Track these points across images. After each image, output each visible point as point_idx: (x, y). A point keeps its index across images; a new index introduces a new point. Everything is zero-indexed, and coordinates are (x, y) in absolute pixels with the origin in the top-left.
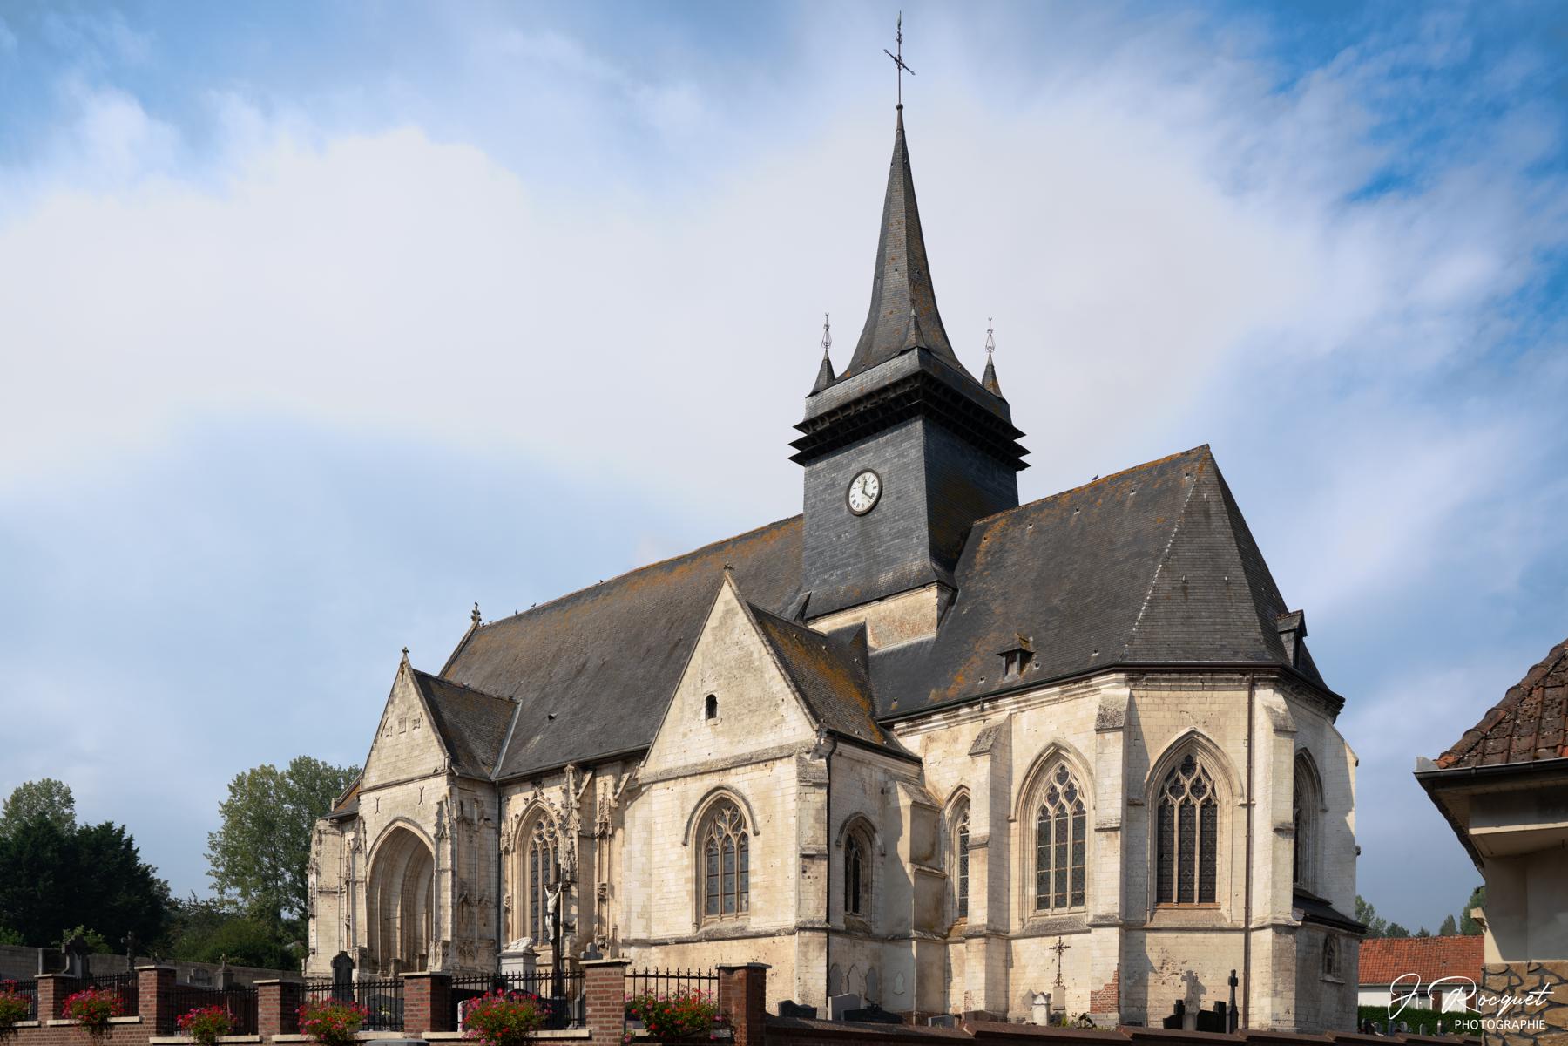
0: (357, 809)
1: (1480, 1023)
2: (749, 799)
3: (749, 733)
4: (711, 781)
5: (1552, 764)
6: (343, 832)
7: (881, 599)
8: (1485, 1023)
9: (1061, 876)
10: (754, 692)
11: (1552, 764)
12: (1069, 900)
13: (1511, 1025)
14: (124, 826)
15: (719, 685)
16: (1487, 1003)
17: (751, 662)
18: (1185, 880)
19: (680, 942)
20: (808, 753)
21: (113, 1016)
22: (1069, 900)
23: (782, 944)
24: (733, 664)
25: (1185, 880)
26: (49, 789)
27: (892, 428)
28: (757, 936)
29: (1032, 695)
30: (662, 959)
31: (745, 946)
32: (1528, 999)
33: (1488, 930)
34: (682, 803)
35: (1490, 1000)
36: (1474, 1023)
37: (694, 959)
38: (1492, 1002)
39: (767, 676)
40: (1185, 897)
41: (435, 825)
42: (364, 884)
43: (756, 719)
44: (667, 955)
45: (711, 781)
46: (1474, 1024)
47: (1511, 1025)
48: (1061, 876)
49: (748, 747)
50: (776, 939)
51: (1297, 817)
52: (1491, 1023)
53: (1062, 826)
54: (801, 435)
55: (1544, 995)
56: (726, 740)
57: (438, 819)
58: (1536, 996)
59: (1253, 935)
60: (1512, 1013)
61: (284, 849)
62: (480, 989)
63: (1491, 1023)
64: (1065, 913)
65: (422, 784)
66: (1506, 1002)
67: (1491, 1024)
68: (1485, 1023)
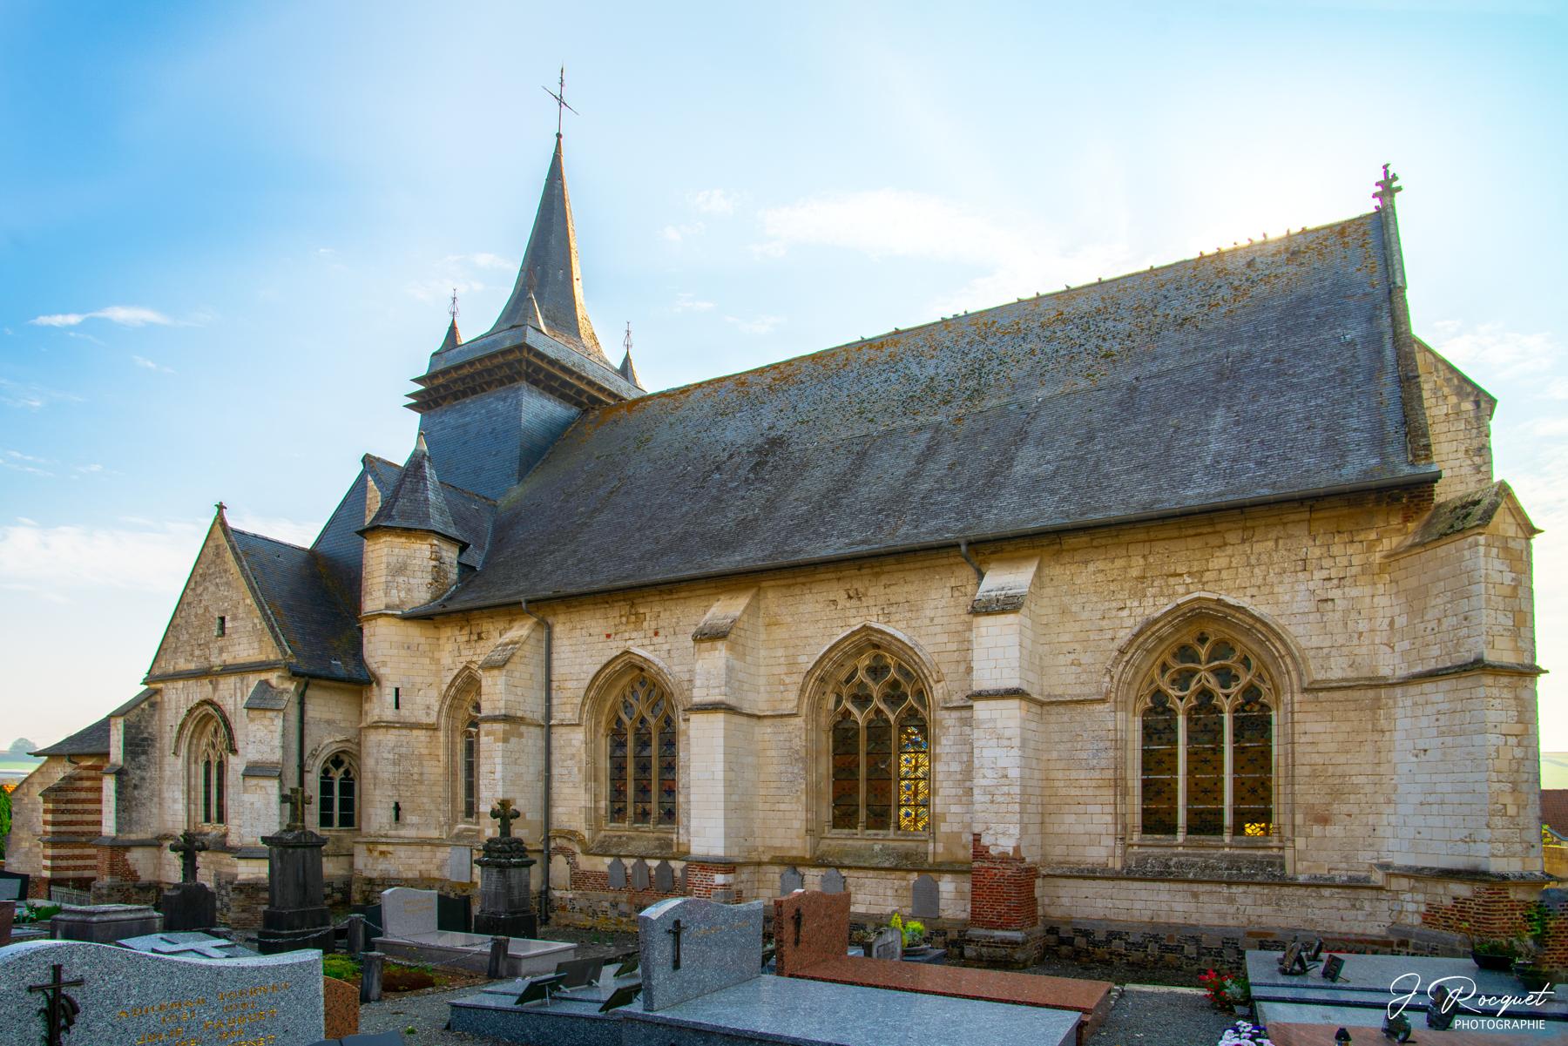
0: (424, 432)
1: (1480, 1023)
6: (981, 575)
8: (1485, 1023)
9: (643, 767)
13: (1511, 1025)
14: (1547, 672)
16: (1487, 1003)
20: (765, 946)
32: (1528, 999)
33: (146, 687)
35: (1490, 1000)
38: (1493, 1001)
41: (1303, 229)
46: (1474, 1025)
47: (1511, 1025)
48: (643, 767)
54: (420, 387)
58: (1536, 997)
59: (554, 730)
68: (1485, 1023)
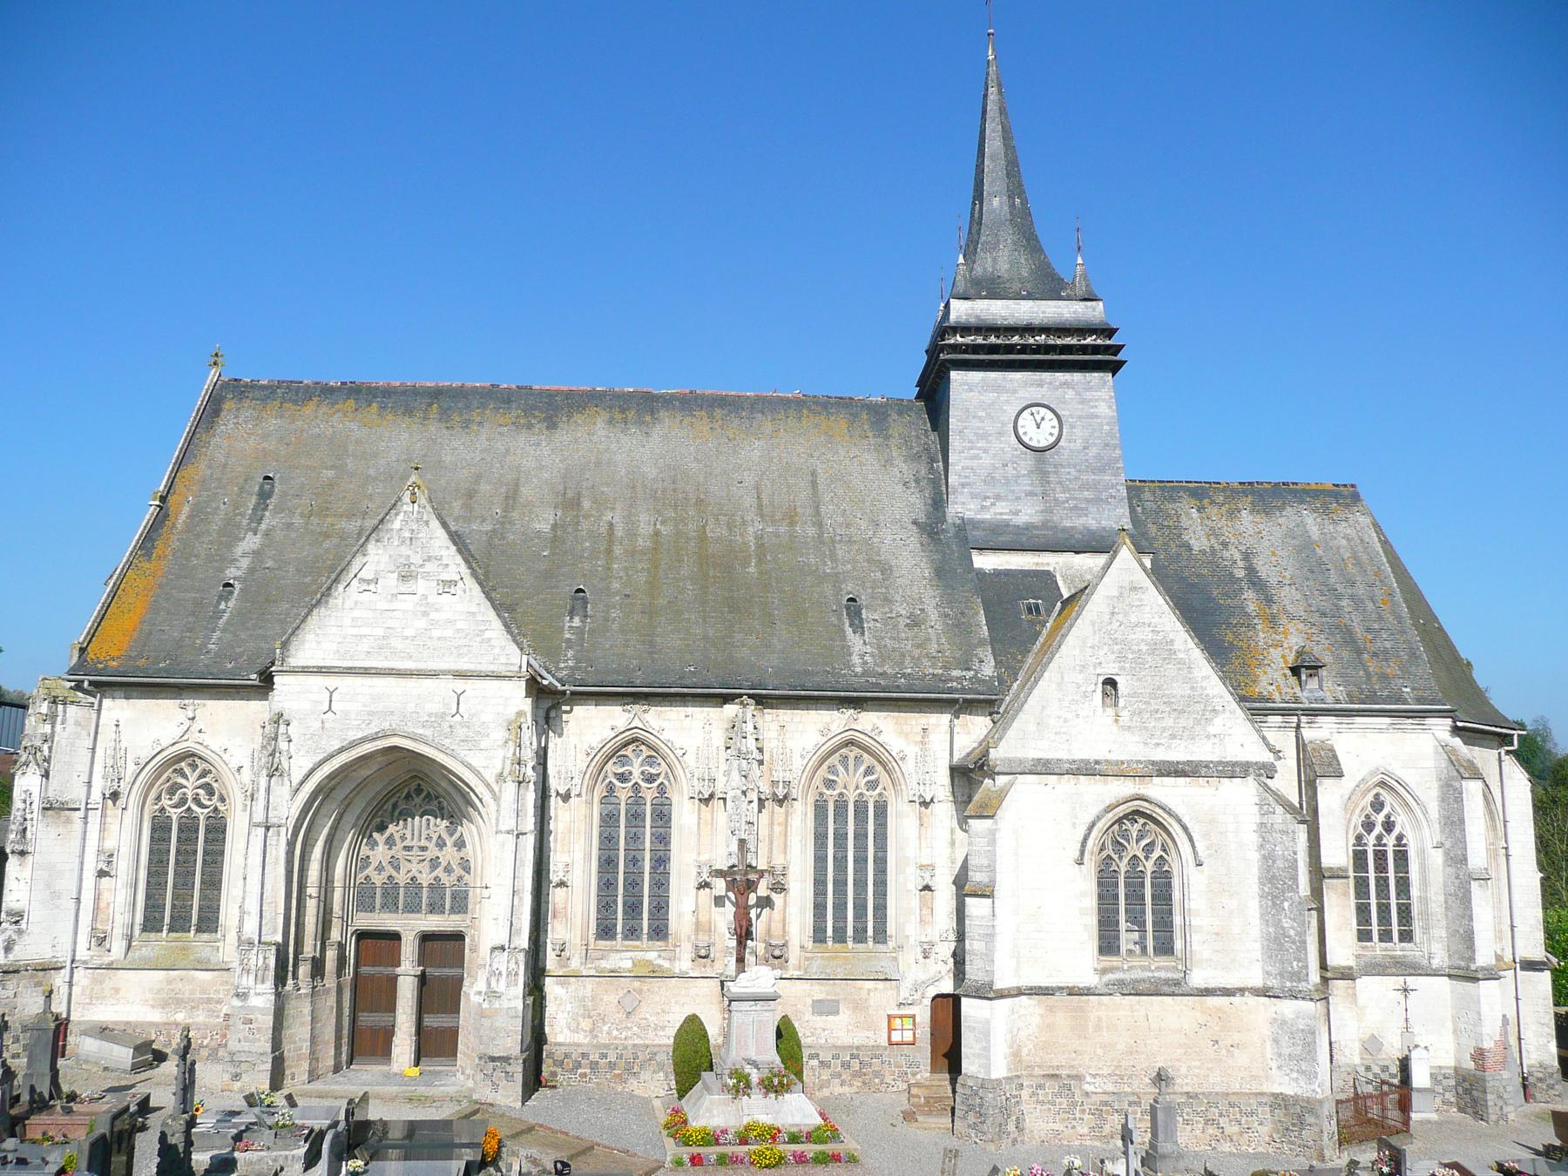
2: (1186, 820)
3: (1173, 737)
4: (1126, 788)
7: (1077, 553)
10: (1179, 690)
12: (378, 906)
15: (1122, 668)
17: (1172, 652)
18: (633, 909)
19: (1073, 992)
22: (378, 906)
23: (1244, 1008)
24: (1144, 648)
25: (633, 909)
26: (1542, 718)
28: (1207, 992)
29: (1358, 719)
30: (1042, 1016)
31: (1187, 1006)
34: (1074, 809)
37: (1099, 1019)
39: (1197, 673)
40: (632, 933)
42: (283, 830)
43: (1183, 722)
44: (1051, 1009)
45: (1126, 788)
49: (1178, 753)
50: (1236, 999)
53: (1380, 856)
56: (1136, 738)
64: (1397, 948)
65: (460, 685)
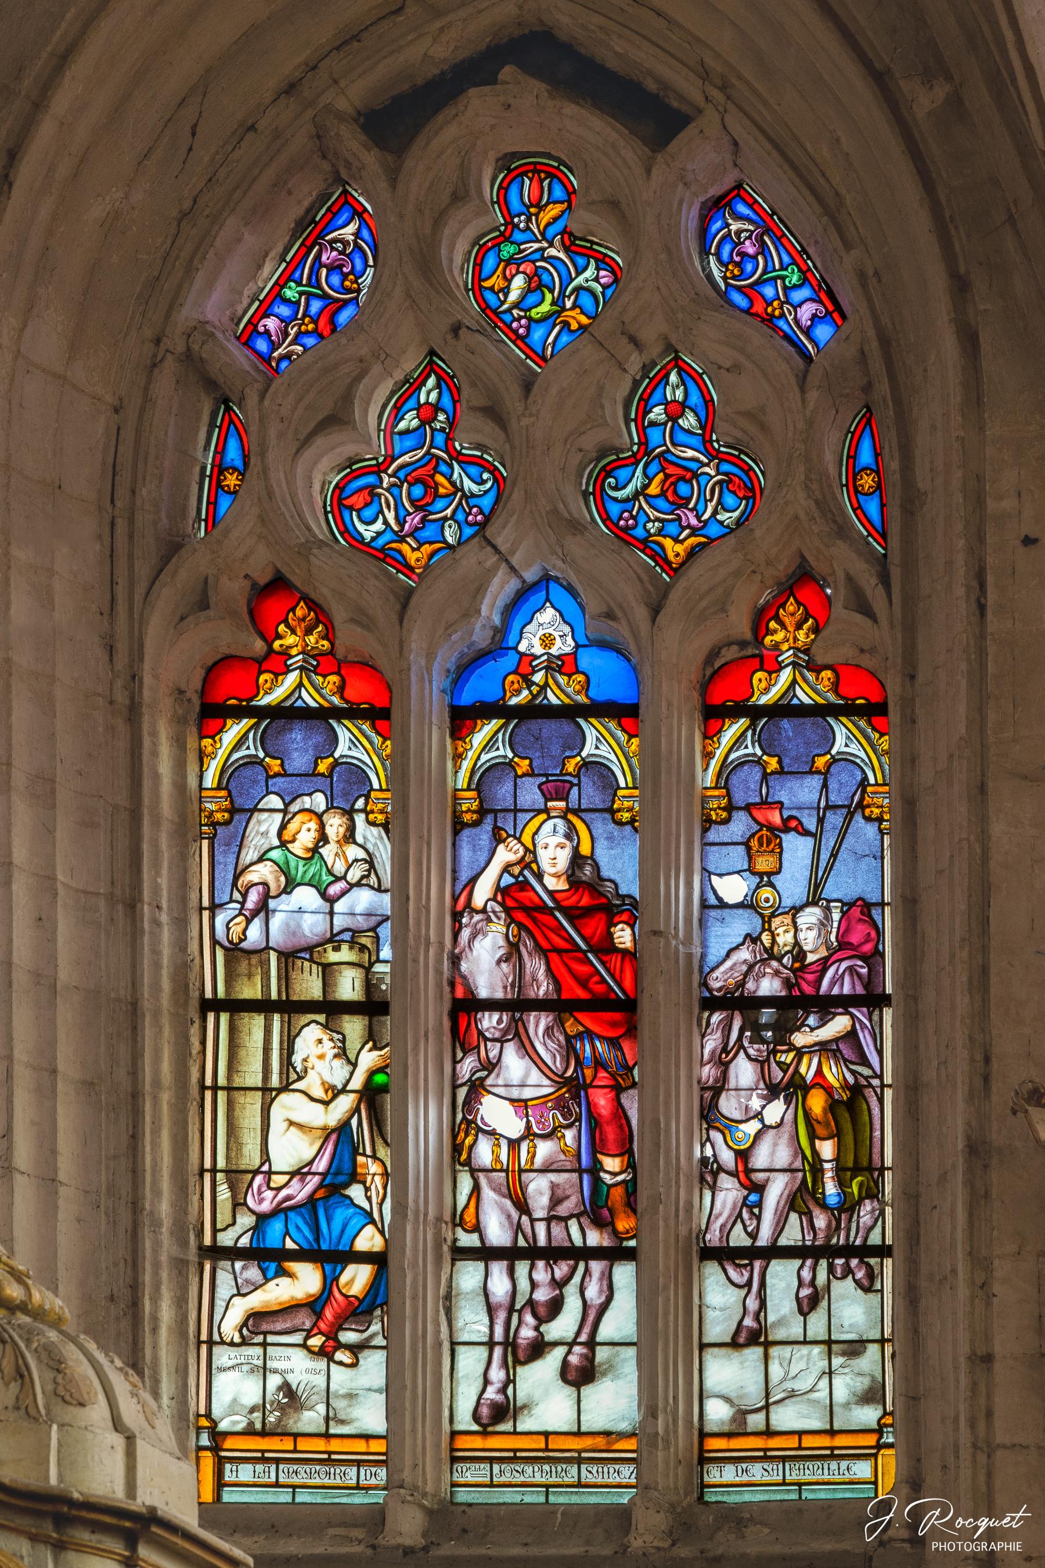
1: (957, 1545)
5: (896, 1282)
8: (962, 1545)
11: (896, 1282)
21: (315, 1191)
27: (406, 87)
32: (1005, 1521)
36: (951, 1546)
38: (970, 1523)
51: (387, 1385)
52: (968, 1545)
55: (1021, 1518)
57: (46, 1543)
60: (991, 1534)
61: (833, 1106)
62: (257, 1466)
63: (968, 1545)
66: (984, 1523)
67: (968, 1546)
68: (962, 1545)
